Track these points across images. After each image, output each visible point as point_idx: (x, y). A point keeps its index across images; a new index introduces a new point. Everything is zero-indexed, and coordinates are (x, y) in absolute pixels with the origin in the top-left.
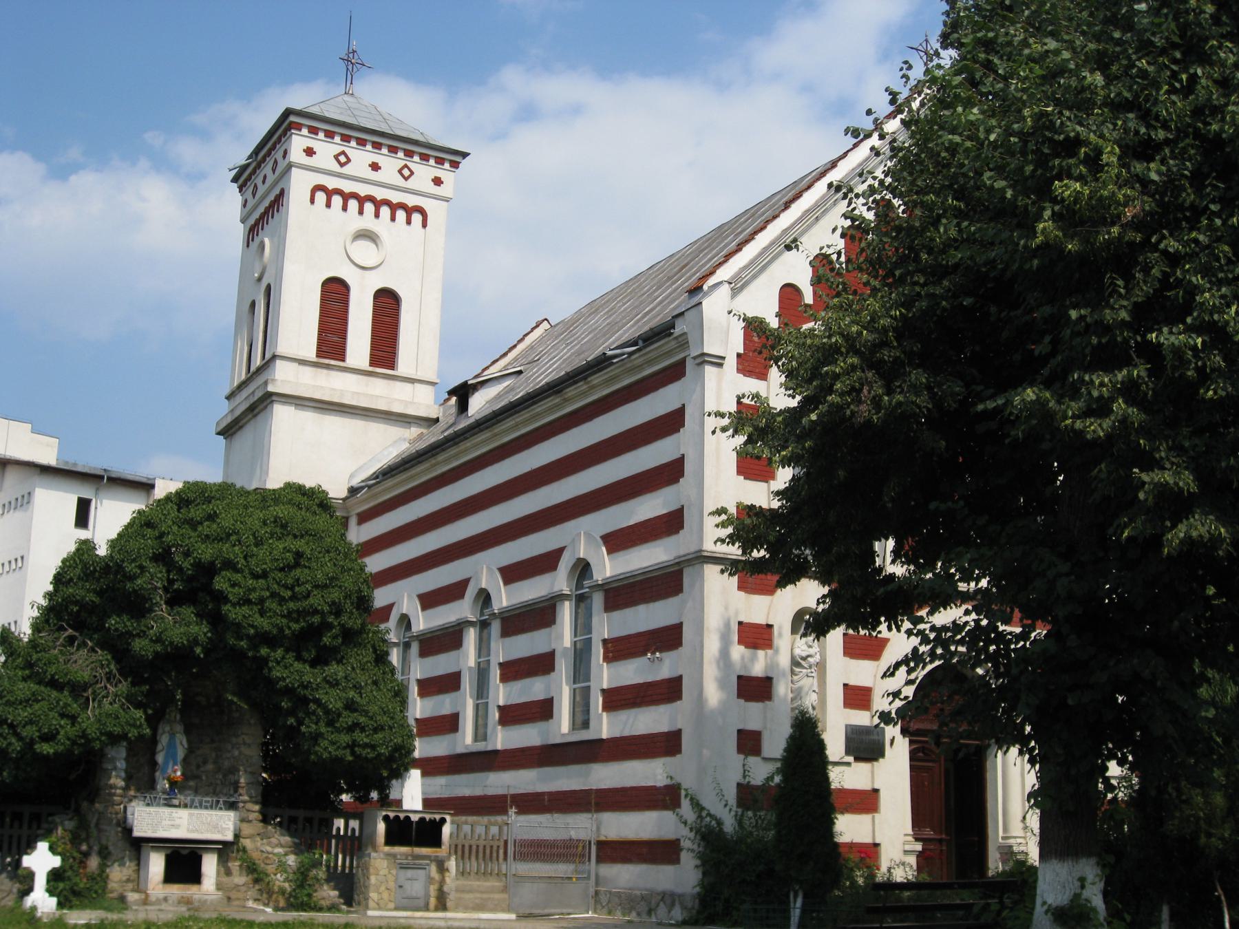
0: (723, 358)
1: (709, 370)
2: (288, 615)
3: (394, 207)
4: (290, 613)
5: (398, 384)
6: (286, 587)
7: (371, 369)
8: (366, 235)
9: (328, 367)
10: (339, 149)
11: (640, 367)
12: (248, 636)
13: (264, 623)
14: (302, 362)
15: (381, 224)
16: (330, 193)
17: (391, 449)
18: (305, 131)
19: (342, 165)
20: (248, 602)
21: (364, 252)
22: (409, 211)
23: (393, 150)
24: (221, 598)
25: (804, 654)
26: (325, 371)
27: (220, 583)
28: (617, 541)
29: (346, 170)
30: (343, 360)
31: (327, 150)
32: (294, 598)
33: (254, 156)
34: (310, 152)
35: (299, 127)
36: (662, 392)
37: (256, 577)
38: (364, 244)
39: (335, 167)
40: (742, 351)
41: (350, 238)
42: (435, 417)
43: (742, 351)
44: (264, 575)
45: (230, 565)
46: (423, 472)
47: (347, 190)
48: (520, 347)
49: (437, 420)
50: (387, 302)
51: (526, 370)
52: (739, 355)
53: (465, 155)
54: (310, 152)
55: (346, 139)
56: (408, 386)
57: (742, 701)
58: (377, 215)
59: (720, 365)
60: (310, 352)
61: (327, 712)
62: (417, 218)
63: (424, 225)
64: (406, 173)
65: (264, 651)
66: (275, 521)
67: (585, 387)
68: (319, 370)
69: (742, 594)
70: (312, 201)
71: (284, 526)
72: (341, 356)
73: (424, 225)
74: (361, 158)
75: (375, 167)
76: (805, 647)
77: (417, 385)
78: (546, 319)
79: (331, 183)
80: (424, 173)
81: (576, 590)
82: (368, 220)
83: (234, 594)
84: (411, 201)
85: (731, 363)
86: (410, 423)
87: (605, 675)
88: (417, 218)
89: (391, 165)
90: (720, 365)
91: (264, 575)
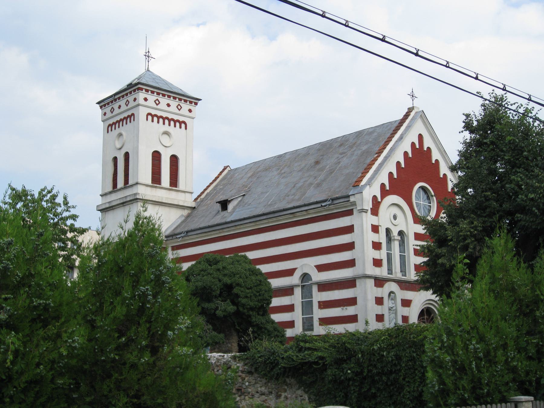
0: (368, 210)
1: (364, 214)
2: (258, 301)
3: (175, 121)
4: (259, 300)
5: (180, 194)
6: (257, 292)
7: (171, 188)
8: (166, 133)
9: (156, 187)
10: (156, 98)
11: (333, 209)
12: (247, 308)
13: (252, 304)
14: (147, 185)
15: (171, 129)
16: (153, 116)
17: (178, 220)
18: (144, 91)
19: (157, 105)
20: (247, 297)
21: (165, 140)
22: (181, 123)
23: (175, 98)
24: (237, 296)
25: (392, 306)
26: (154, 189)
27: (236, 290)
28: (321, 268)
29: (159, 107)
30: (176, 187)
31: (152, 98)
32: (260, 295)
33: (113, 96)
34: (146, 99)
35: (142, 89)
36: (341, 219)
37: (248, 289)
38: (166, 136)
39: (155, 106)
40: (372, 207)
41: (161, 134)
42: (194, 206)
43: (372, 207)
44: (251, 288)
45: (238, 285)
46: (214, 234)
47: (159, 115)
48: (221, 177)
49: (195, 208)
50: (174, 160)
51: (246, 194)
52: (371, 208)
53: (200, 100)
54: (146, 99)
55: (158, 94)
56: (183, 194)
57: (377, 322)
58: (169, 125)
59: (366, 212)
60: (149, 182)
61: (269, 331)
62: (183, 125)
63: (186, 128)
64: (179, 108)
65: (251, 313)
66: (249, 270)
67: (305, 213)
68: (153, 188)
69: (375, 288)
70: (147, 120)
71: (252, 272)
72: (160, 183)
73: (186, 128)
74: (164, 101)
75: (169, 105)
76: (391, 304)
77: (187, 194)
78: (229, 166)
79: (154, 112)
80: (186, 107)
81: (301, 283)
82: (166, 128)
83: (242, 294)
84: (181, 119)
85: (369, 211)
86: (184, 209)
87: (318, 314)
88: (183, 125)
89: (174, 104)
90: (366, 212)
91: (251, 288)
